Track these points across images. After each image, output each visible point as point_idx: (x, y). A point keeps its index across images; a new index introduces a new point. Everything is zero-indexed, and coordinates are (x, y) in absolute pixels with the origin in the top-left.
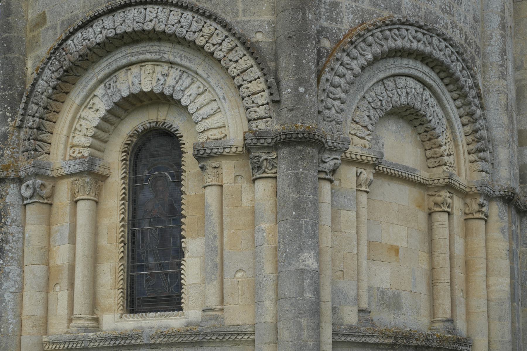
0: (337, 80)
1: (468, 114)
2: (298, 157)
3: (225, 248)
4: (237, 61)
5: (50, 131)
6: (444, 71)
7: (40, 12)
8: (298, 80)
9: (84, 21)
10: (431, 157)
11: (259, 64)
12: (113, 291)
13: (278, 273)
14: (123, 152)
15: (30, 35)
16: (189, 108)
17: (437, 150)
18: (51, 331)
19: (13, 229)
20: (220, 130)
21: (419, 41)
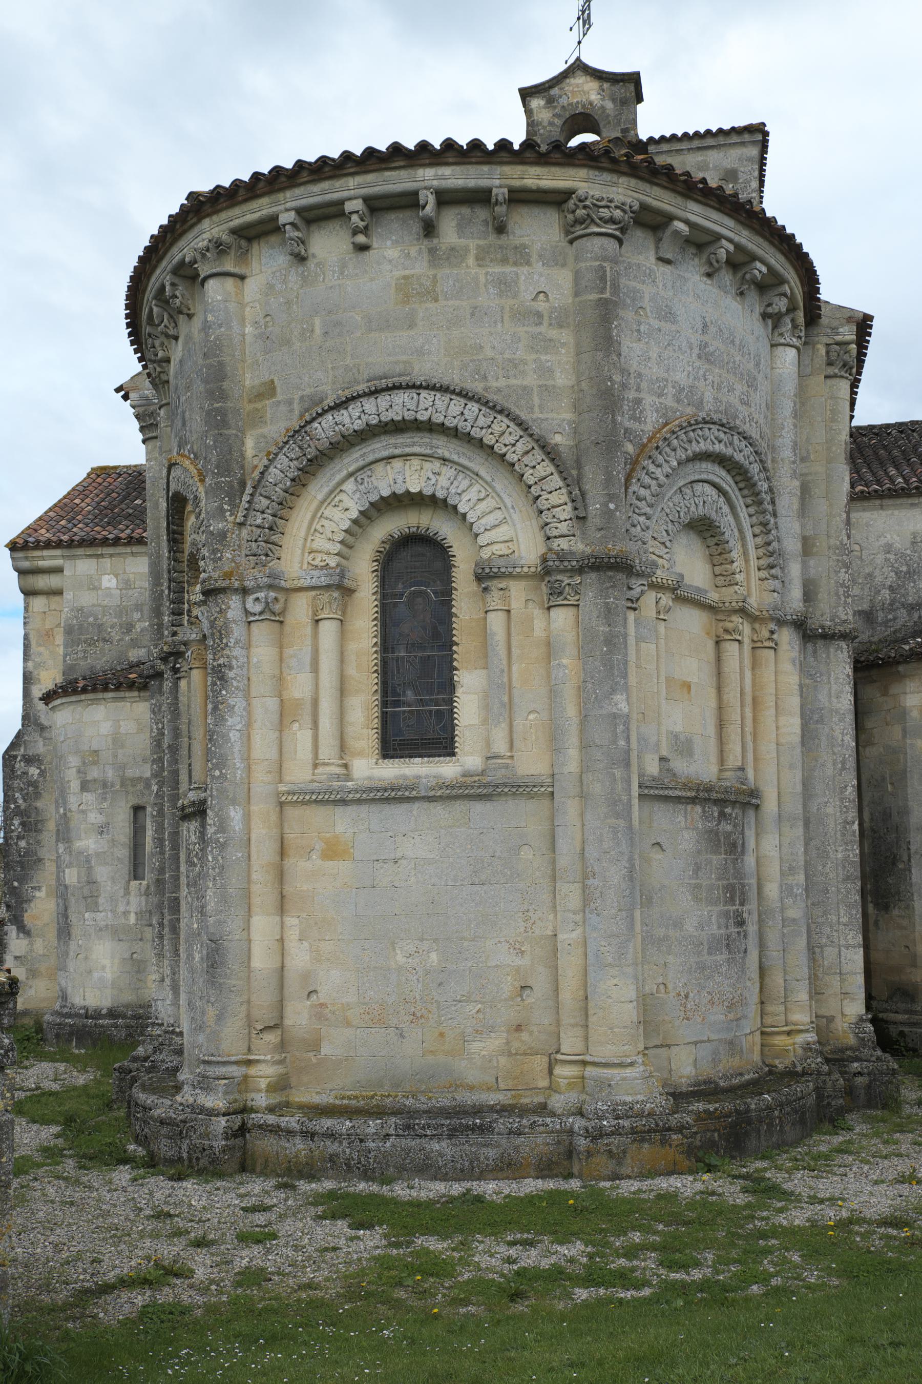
1: (761, 524)
2: (608, 585)
3: (514, 684)
4: (534, 467)
5: (282, 531)
6: (740, 474)
7: (267, 378)
8: (608, 495)
9: (337, 402)
10: (720, 575)
11: (561, 472)
12: (365, 731)
13: (584, 719)
14: (374, 561)
15: (249, 407)
16: (468, 516)
17: (728, 566)
18: (287, 778)
19: (237, 652)
20: (507, 544)
21: (720, 442)
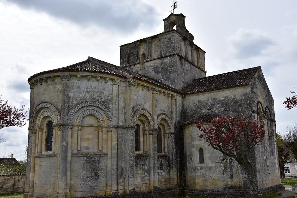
0: (72, 113)
